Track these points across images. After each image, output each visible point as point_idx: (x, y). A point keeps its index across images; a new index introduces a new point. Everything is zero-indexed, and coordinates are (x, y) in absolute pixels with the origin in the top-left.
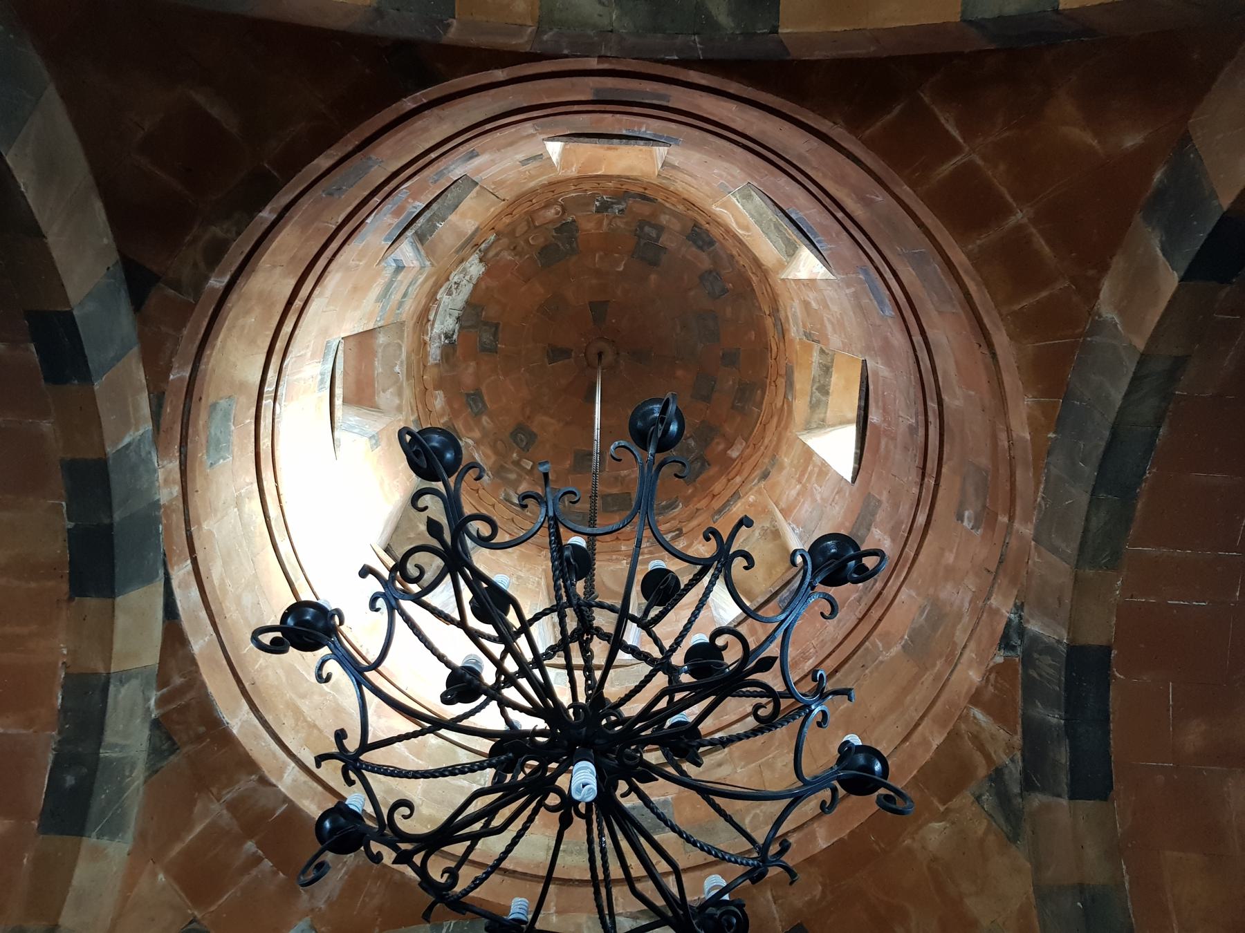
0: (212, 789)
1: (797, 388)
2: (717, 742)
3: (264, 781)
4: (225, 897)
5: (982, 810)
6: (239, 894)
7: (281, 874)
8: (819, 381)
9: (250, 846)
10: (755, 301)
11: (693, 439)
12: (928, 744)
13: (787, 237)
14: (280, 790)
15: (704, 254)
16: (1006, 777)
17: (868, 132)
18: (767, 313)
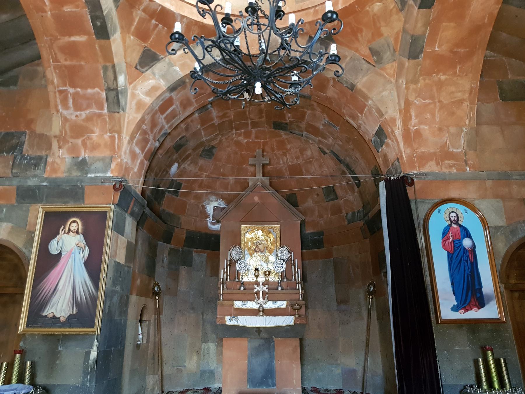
2: (142, 212)
6: (155, 36)
9: (154, 22)
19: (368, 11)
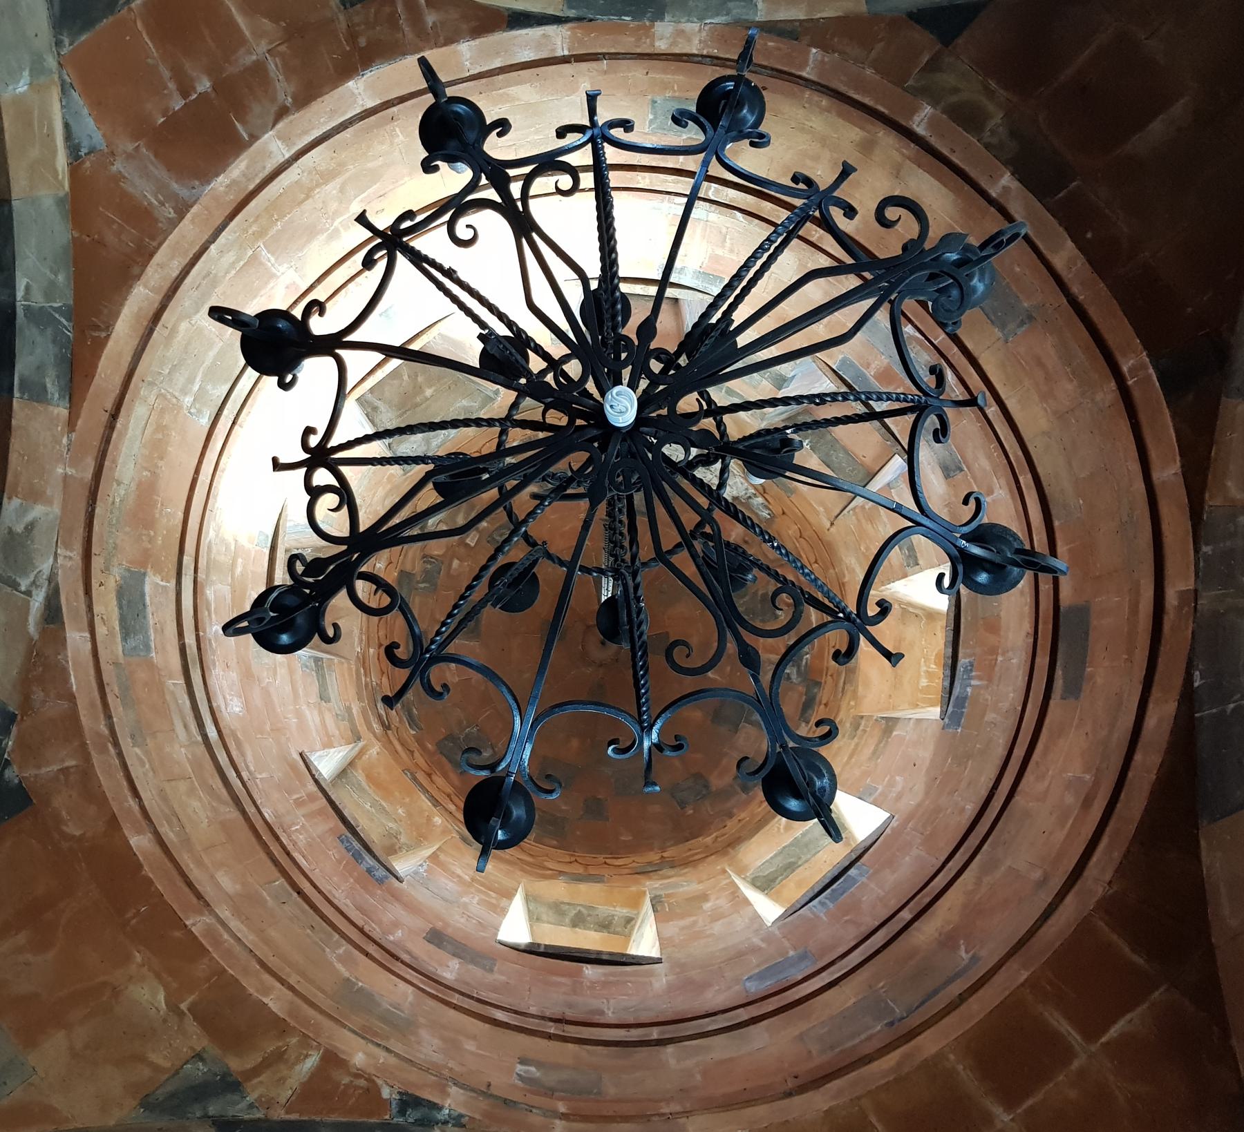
0: (286, 45)
1: (581, 886)
3: (282, 113)
4: (149, 42)
5: (184, 1061)
7: (162, 120)
8: (589, 915)
10: (672, 842)
11: (492, 755)
12: (266, 994)
13: (777, 878)
14: (267, 132)
15: (731, 779)
16: (229, 1097)
17: (1101, 924)
18: (665, 854)
19: (128, 958)
